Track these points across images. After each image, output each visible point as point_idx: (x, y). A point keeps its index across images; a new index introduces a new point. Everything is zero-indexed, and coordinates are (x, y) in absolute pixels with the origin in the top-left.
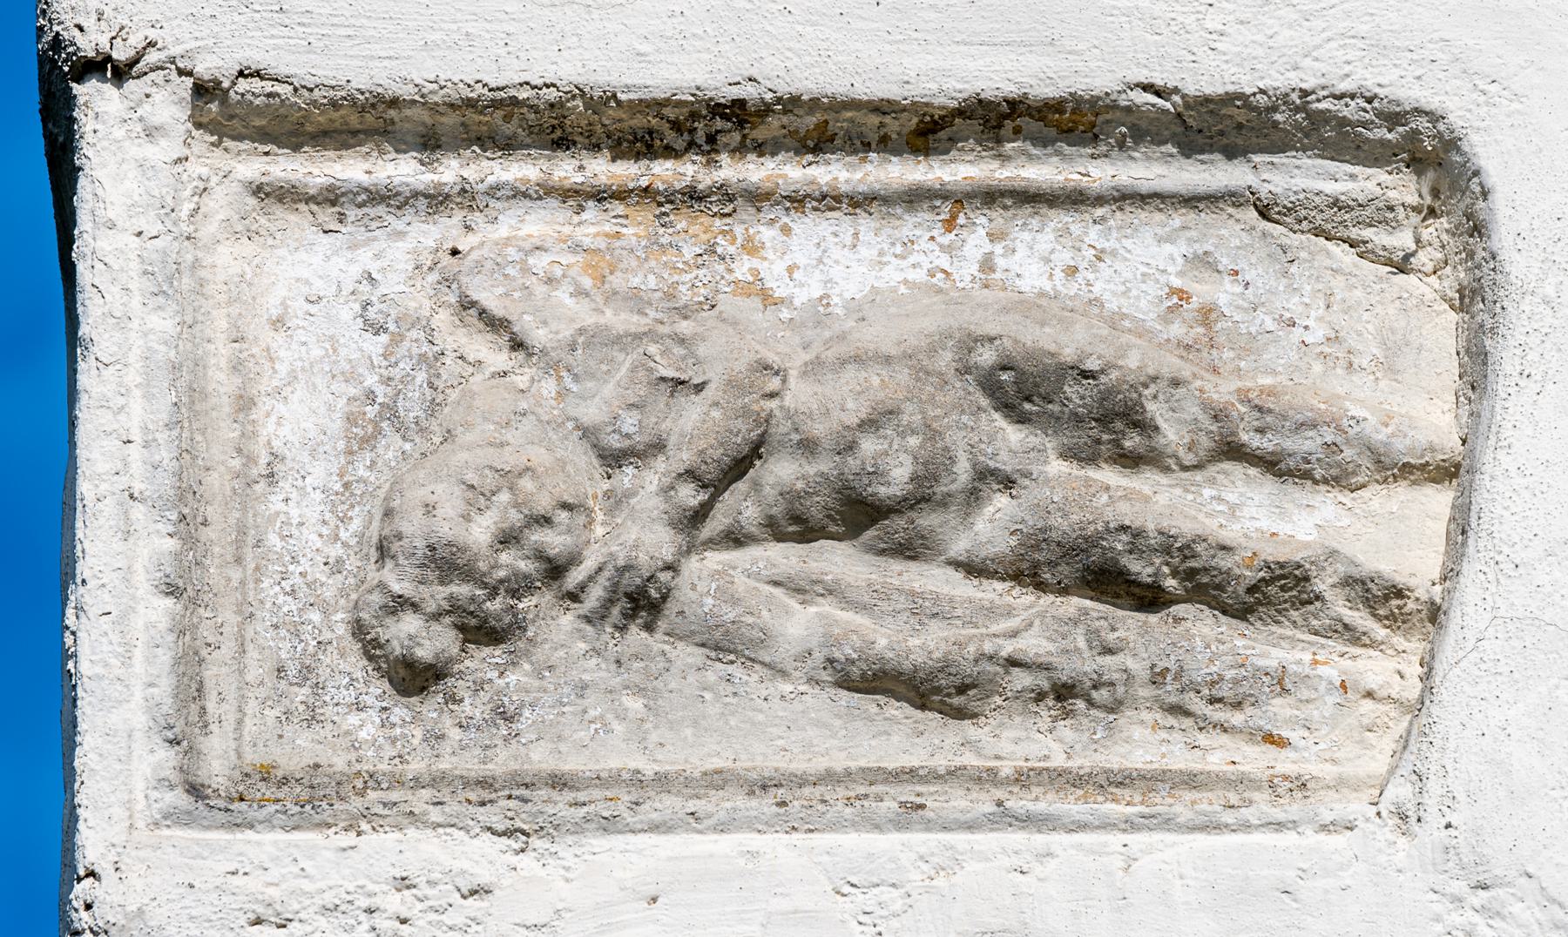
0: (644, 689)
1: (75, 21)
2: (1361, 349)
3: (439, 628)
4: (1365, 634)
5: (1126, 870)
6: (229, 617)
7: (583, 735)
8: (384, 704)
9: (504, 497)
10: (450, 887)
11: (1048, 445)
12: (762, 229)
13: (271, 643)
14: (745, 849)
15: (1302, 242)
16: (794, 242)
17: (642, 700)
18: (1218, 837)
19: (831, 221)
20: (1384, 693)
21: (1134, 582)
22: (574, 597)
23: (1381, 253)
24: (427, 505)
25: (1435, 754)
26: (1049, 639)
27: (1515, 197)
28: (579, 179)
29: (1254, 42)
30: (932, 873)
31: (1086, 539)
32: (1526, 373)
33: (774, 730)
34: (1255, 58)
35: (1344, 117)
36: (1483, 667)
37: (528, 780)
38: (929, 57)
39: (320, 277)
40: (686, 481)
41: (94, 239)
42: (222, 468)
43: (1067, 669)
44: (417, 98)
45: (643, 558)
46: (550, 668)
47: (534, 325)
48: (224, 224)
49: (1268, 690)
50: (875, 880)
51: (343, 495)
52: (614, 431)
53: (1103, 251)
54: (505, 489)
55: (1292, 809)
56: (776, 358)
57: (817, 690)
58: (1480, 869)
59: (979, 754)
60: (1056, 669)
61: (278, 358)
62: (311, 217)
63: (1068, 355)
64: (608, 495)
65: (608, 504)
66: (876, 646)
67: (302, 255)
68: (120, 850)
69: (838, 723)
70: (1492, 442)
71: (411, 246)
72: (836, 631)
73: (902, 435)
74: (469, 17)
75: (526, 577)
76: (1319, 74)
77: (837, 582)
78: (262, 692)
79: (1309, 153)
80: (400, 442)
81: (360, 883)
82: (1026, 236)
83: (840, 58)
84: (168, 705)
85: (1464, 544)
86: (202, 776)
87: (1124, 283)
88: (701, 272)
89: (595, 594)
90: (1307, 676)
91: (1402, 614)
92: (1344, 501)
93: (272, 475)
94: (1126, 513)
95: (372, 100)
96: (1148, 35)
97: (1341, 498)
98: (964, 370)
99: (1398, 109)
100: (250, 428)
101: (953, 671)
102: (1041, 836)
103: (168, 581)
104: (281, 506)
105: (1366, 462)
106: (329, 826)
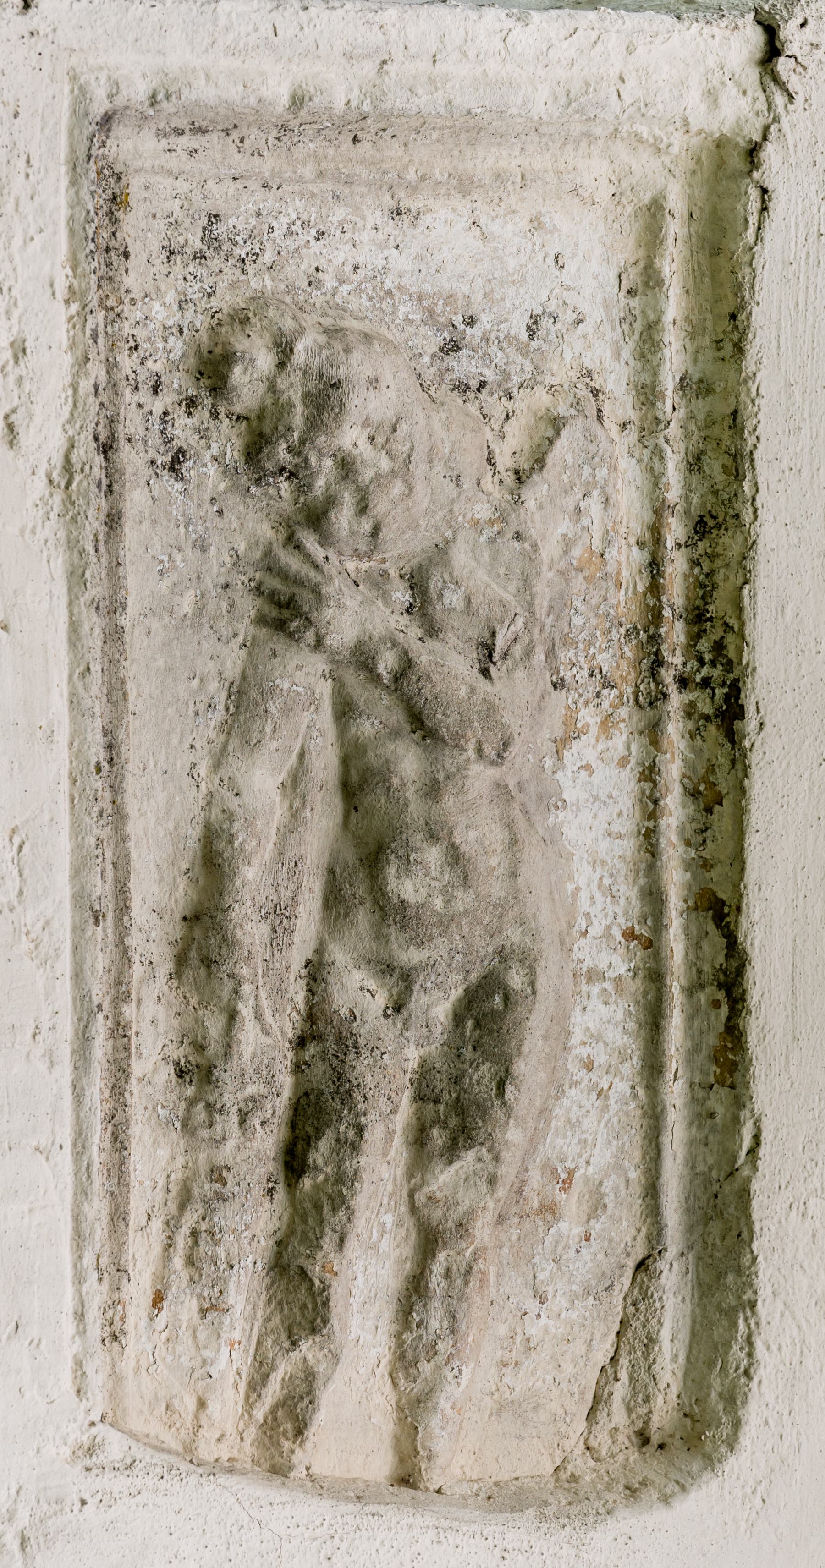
0: (201, 614)
1: (809, 19)
2: (519, 1376)
3: (261, 391)
4: (259, 1396)
5: (37, 1149)
6: (267, 165)
7: (157, 548)
8: (185, 330)
9: (385, 464)
10: (16, 402)
11: (433, 1047)
12: (625, 736)
13: (243, 208)
14: (55, 728)
15: (616, 1307)
16: (614, 771)
17: (190, 611)
18: (68, 1248)
19: (632, 809)
20: (204, 1421)
21: (309, 1145)
22: (292, 542)
23: (606, 1391)
24: (377, 381)
25: (151, 1483)
26: (254, 1055)
27: (663, 1531)
28: (669, 544)
29: (797, 1248)
30: (33, 936)
31: (349, 1093)
32: (506, 1555)
33: (162, 757)
34: (783, 1250)
35: (731, 1347)
36: (235, 1529)
37: (115, 487)
38: (782, 911)
39: (579, 269)
40: (401, 659)
41: (618, 31)
42: (406, 159)
43: (226, 1076)
44: (743, 374)
45: (328, 613)
46: (220, 512)
47: (538, 495)
48: (627, 168)
49: (205, 1294)
50: (26, 872)
51: (382, 288)
52: (445, 582)
53: (607, 1097)
54: (392, 465)
55: (95, 1330)
56: (513, 754)
57: (202, 803)
58: (41, 1539)
59: (142, 981)
60: (226, 1063)
61: (506, 222)
62: (632, 260)
63: (520, 1067)
64: (384, 574)
65: (376, 574)
66: (247, 867)
67: (598, 251)
68: (50, 38)
69: (171, 826)
70: (445, 1524)
71: (607, 365)
72: (258, 823)
73: (444, 891)
74: (814, 430)
75: (310, 486)
76: (770, 1319)
77: (304, 822)
78: (196, 197)
79: (697, 1311)
80: (430, 351)
81: (20, 303)
82: (620, 1015)
83: (781, 818)
84: (189, 95)
85: (347, 1499)
86: (119, 130)
87: (578, 1120)
88: (585, 673)
89: (292, 562)
90: (219, 1336)
91: (278, 1434)
92: (381, 1365)
93: (399, 214)
94: (375, 1134)
95: (741, 327)
96: (801, 1139)
97: (384, 1362)
98: (503, 955)
99: (739, 1403)
100: (443, 191)
101: (224, 952)
102: (69, 1056)
103: (306, 99)
104: (370, 224)
105: (418, 1387)
106: (74, 268)
